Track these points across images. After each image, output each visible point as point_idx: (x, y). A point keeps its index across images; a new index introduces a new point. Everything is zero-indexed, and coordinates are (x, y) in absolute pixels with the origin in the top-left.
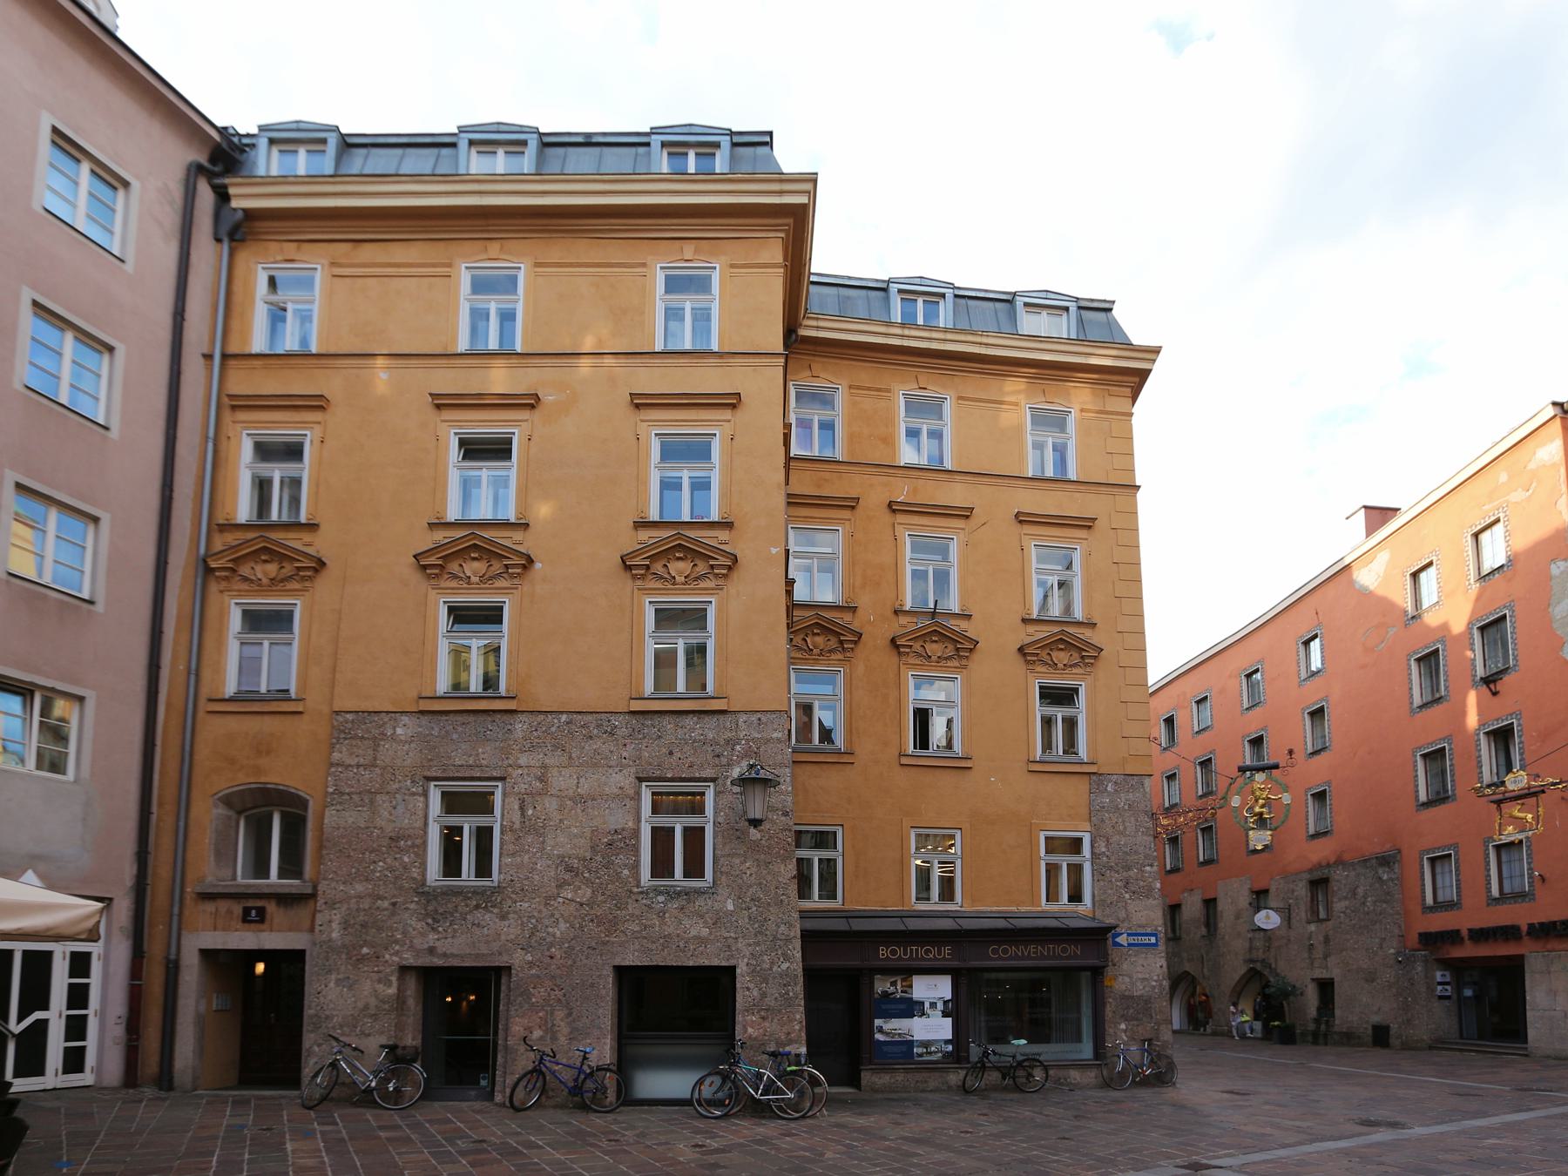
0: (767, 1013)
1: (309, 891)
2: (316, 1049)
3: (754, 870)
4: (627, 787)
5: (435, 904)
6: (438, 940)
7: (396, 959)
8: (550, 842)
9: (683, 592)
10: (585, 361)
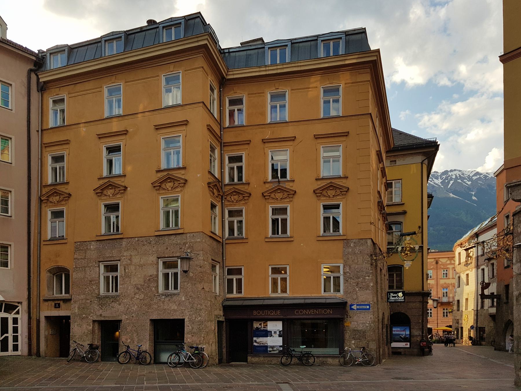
0: (193, 334)
1: (70, 298)
2: (72, 345)
3: (191, 286)
4: (154, 260)
5: (102, 300)
6: (102, 312)
7: (92, 318)
8: (132, 280)
9: (171, 193)
10: (140, 115)
